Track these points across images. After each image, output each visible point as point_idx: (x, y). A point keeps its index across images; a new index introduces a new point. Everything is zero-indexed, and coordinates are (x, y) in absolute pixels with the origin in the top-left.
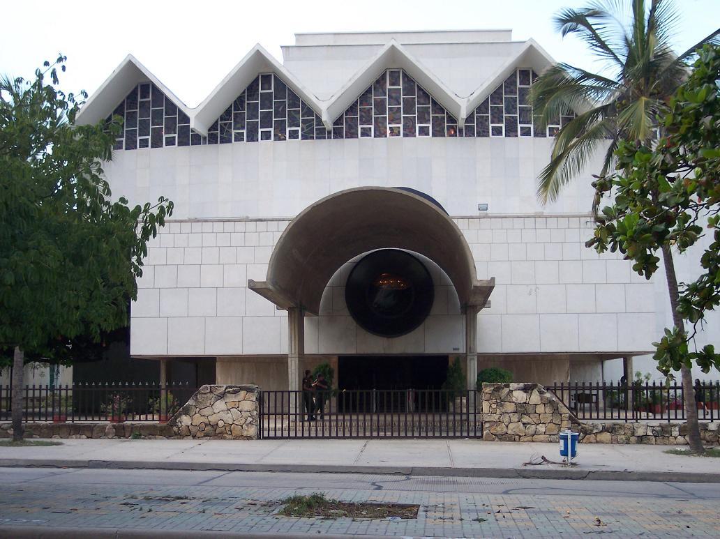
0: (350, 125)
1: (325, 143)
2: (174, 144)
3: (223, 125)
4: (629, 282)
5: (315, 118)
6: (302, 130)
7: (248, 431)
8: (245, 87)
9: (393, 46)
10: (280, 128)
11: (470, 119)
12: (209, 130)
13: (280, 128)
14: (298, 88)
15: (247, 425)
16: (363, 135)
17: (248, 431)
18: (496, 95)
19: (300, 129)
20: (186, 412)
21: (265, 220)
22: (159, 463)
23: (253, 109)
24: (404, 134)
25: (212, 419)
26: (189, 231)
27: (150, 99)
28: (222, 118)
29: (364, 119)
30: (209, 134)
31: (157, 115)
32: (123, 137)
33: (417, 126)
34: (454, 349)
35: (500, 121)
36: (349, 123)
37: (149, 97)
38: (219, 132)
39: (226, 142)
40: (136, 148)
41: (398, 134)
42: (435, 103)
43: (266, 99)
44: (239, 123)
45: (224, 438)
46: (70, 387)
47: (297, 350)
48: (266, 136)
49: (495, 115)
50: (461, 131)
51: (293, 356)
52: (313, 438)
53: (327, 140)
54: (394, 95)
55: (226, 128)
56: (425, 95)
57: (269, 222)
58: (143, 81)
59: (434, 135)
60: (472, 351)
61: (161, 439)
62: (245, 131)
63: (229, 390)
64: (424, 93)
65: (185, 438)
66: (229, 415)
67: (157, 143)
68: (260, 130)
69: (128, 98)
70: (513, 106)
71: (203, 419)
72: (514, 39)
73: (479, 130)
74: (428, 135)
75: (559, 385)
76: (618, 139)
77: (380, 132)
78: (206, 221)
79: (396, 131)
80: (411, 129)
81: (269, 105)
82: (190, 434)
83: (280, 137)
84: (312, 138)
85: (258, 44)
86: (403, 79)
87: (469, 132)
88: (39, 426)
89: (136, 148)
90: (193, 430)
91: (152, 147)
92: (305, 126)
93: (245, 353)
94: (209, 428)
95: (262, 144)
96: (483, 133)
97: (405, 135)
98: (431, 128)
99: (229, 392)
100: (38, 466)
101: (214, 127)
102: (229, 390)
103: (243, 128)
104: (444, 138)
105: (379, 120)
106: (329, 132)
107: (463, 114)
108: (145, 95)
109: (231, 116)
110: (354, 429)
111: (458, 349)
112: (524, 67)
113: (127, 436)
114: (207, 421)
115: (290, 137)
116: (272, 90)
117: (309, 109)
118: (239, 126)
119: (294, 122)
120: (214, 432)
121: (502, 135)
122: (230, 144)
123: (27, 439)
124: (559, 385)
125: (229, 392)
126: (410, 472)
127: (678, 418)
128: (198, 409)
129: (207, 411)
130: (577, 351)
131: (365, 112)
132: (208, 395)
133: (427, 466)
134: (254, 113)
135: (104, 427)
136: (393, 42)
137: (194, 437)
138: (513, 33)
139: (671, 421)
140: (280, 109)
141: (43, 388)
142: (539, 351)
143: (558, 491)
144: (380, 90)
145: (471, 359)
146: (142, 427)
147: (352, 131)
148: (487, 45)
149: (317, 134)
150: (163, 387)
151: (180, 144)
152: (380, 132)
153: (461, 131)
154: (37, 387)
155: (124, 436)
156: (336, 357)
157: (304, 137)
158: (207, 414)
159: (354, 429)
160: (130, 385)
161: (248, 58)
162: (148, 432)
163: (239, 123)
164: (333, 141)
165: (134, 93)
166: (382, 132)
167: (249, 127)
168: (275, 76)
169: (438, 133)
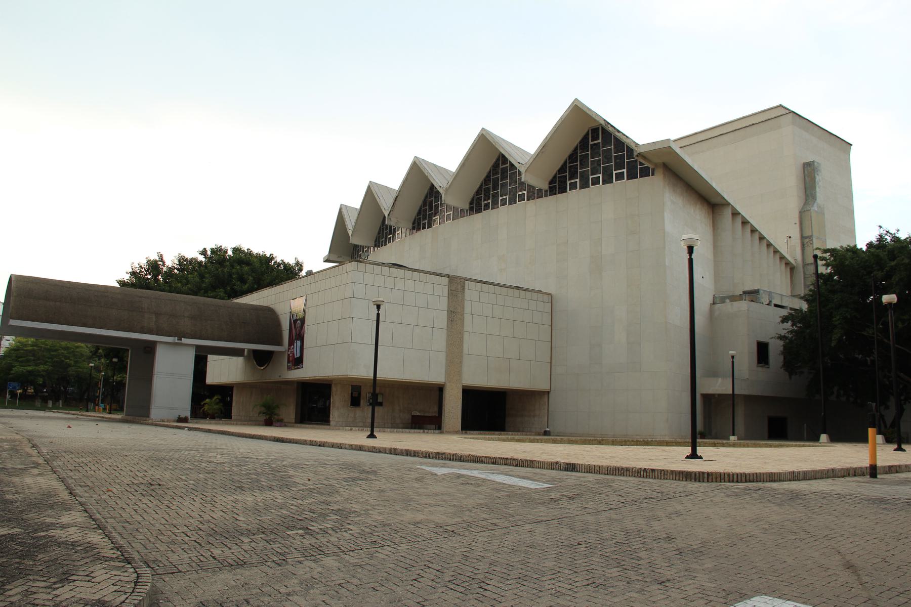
4: (540, 325)
30: (550, 187)
32: (625, 169)
40: (650, 176)
49: (486, 194)
58: (593, 125)
67: (608, 180)
85: (483, 128)
93: (190, 409)
101: (471, 203)
106: (546, 191)
108: (595, 138)
121: (599, 184)
126: (494, 461)
156: (155, 413)
157: (604, 182)
163: (573, 175)
164: (549, 198)
165: (585, 139)
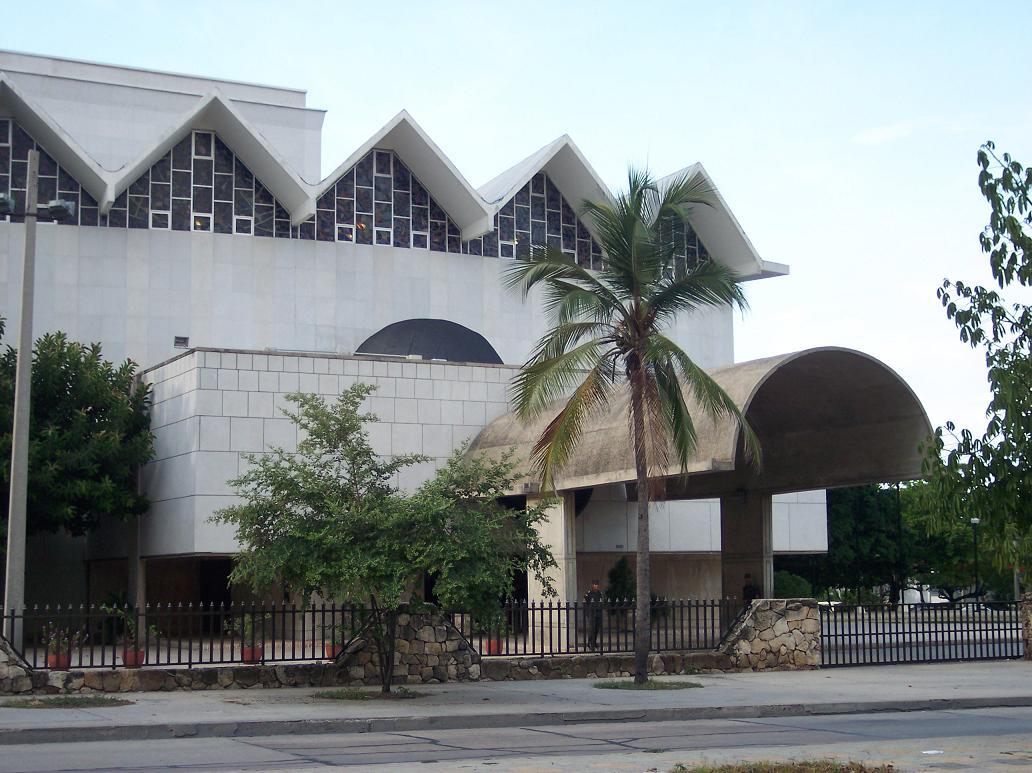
0: (323, 221)
1: (288, 243)
3: (134, 200)
6: (256, 221)
7: (812, 658)
9: (216, 98)
10: (224, 215)
11: (120, 199)
13: (224, 215)
14: (159, 148)
16: (341, 237)
17: (812, 658)
18: (157, 167)
19: (252, 219)
20: (745, 635)
21: (217, 351)
22: (896, 703)
23: (182, 183)
24: (394, 242)
25: (774, 644)
26: (413, 375)
27: (10, 144)
29: (342, 216)
33: (412, 233)
34: (618, 547)
35: (510, 238)
36: (323, 218)
38: (320, 229)
39: (140, 227)
41: (388, 242)
42: (434, 204)
43: (203, 169)
45: (787, 669)
46: (19, 612)
49: (505, 229)
50: (465, 246)
52: (888, 663)
53: (291, 241)
54: (382, 186)
55: (139, 204)
56: (421, 193)
57: (286, 358)
59: (432, 248)
62: (169, 213)
63: (791, 605)
64: (421, 189)
65: (744, 670)
66: (792, 638)
70: (525, 219)
71: (764, 645)
72: (308, 105)
73: (135, 216)
74: (249, 231)
75: (678, 603)
77: (363, 237)
78: (304, 356)
79: (385, 237)
80: (404, 236)
82: (752, 665)
83: (223, 227)
84: (271, 235)
86: (395, 166)
87: (116, 219)
88: (711, 657)
90: (754, 659)
92: (259, 217)
93: (672, 550)
96: (139, 223)
97: (397, 244)
98: (392, 234)
99: (791, 609)
100: (623, 720)
102: (791, 605)
104: (74, 227)
105: (363, 219)
106: (104, 218)
107: (110, 196)
109: (147, 187)
111: (621, 546)
112: (205, 128)
113: (678, 671)
114: (768, 648)
117: (265, 191)
118: (159, 204)
120: (777, 661)
122: (145, 230)
123: (655, 678)
124: (678, 603)
125: (791, 609)
127: (276, 658)
129: (767, 634)
130: (788, 549)
131: (343, 206)
133: (131, 741)
136: (215, 93)
137: (755, 669)
138: (307, 95)
139: (193, 667)
140: (224, 187)
141: (337, 608)
142: (709, 549)
143: (543, 750)
144: (365, 178)
146: (695, 659)
147: (327, 230)
148: (73, 82)
149: (277, 229)
150: (142, 611)
152: (363, 237)
153: (104, 218)
155: (674, 672)
157: (258, 233)
158: (767, 638)
162: (702, 665)
163: (160, 200)
164: (300, 242)
166: (367, 237)
167: (175, 207)
169: (438, 246)
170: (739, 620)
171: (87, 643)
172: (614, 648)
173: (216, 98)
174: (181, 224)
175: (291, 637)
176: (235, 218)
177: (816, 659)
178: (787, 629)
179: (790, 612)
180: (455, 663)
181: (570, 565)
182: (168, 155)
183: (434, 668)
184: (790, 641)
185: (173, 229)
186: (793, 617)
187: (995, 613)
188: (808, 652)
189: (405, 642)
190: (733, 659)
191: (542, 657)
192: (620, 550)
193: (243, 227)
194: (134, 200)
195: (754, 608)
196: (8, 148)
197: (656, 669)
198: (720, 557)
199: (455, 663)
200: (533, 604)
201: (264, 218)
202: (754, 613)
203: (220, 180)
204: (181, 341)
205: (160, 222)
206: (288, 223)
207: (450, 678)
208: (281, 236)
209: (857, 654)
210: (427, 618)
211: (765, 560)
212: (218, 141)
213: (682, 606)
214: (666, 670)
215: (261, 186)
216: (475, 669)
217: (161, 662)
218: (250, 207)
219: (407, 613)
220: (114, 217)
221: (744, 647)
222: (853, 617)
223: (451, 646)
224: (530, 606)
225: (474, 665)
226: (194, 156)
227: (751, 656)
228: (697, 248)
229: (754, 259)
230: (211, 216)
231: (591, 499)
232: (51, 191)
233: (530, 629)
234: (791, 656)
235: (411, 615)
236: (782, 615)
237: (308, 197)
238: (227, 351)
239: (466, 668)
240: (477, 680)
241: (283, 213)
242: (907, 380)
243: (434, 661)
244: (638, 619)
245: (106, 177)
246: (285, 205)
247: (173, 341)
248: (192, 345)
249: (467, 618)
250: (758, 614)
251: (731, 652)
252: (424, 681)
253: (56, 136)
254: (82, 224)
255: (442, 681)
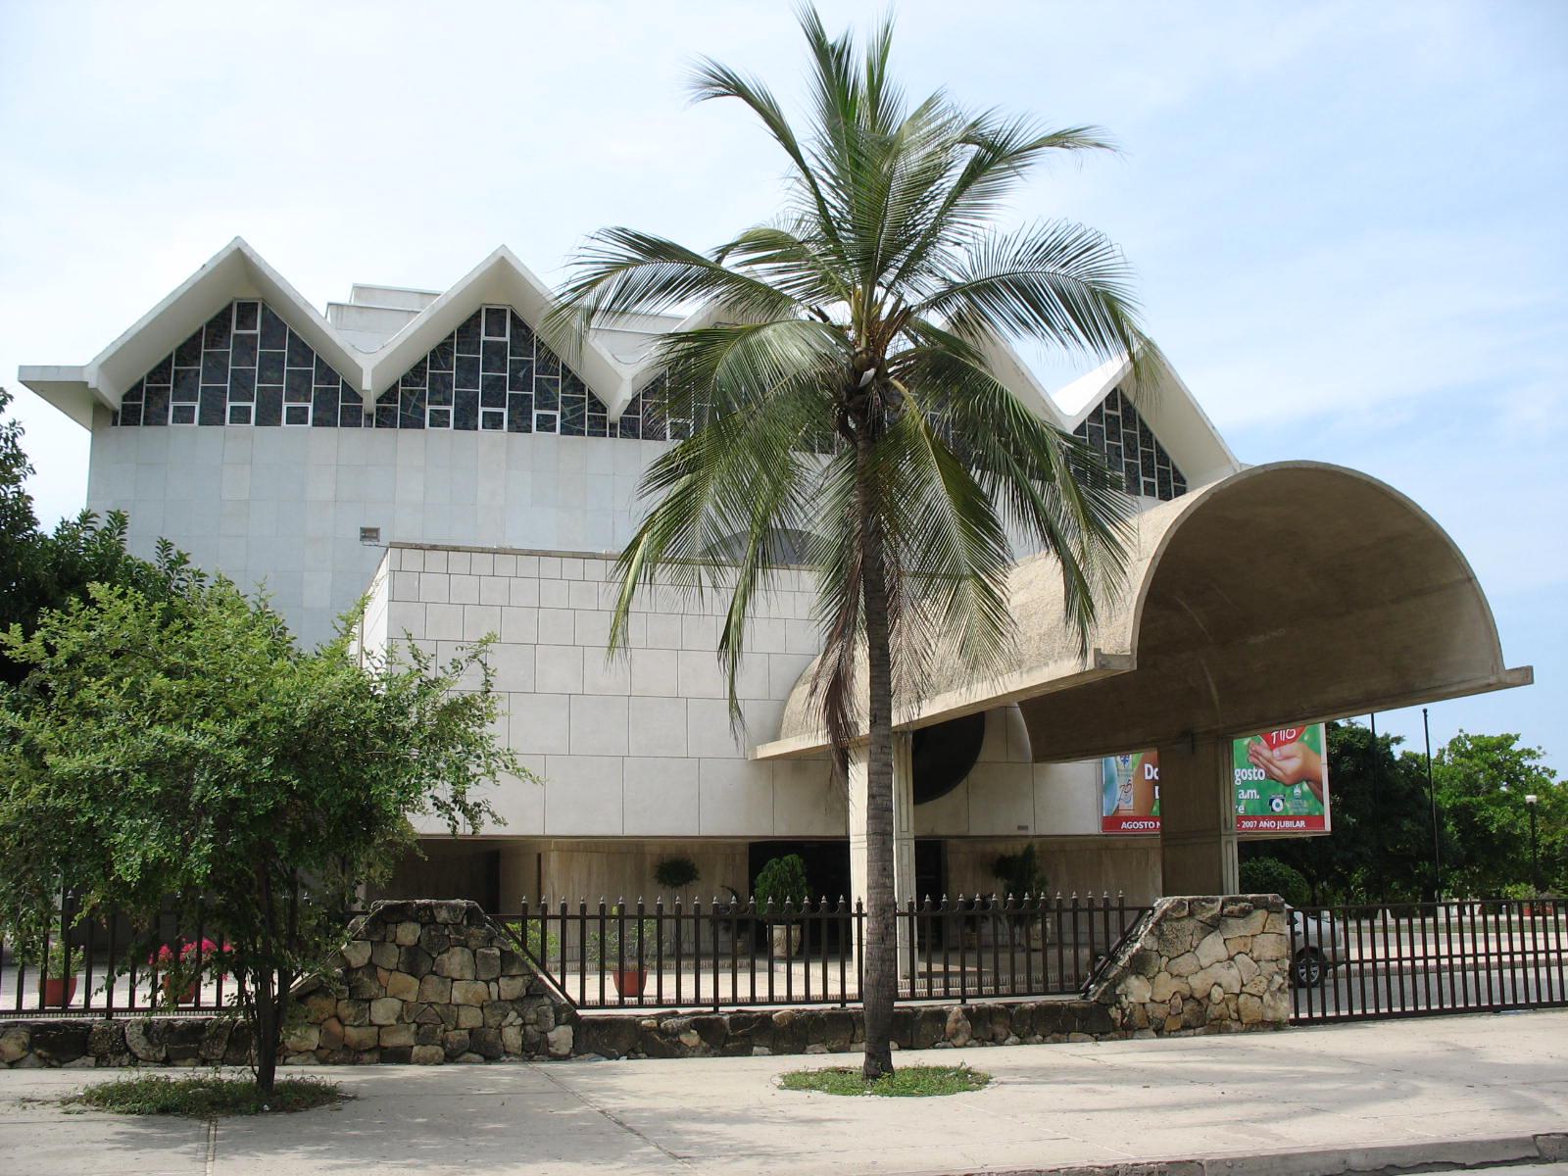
1: (606, 442)
2: (305, 422)
3: (408, 394)
5: (586, 396)
8: (453, 326)
9: (503, 257)
12: (378, 401)
15: (1273, 995)
20: (1140, 965)
23: (468, 369)
25: (1198, 983)
27: (258, 331)
28: (405, 381)
31: (272, 364)
34: (1020, 828)
37: (255, 329)
40: (222, 422)
43: (495, 352)
44: (439, 392)
47: (911, 825)
48: (494, 422)
51: (906, 835)
53: (608, 440)
60: (1229, 826)
61: (992, 1046)
62: (452, 409)
63: (1230, 908)
65: (1137, 1034)
66: (1234, 971)
68: (481, 410)
69: (210, 325)
71: (1176, 985)
76: (128, 588)
81: (499, 364)
83: (520, 425)
84: (581, 433)
87: (384, 418)
89: (222, 422)
91: (257, 424)
92: (567, 410)
94: (1190, 1006)
95: (483, 436)
99: (1231, 915)
102: (1230, 908)
103: (448, 402)
109: (423, 378)
110: (1383, 1001)
111: (1026, 828)
115: (539, 428)
116: (507, 338)
117: (575, 378)
118: (440, 398)
119: (546, 401)
125: (1231, 915)
128: (1165, 960)
129: (1184, 964)
132: (1185, 922)
134: (471, 377)
135: (941, 1016)
137: (1160, 1032)
140: (521, 374)
141: (569, 912)
145: (1227, 843)
149: (590, 426)
151: (317, 422)
154: (593, 910)
158: (1184, 971)
159: (1383, 1001)
160: (814, 905)
161: (484, 269)
167: (459, 401)
168: (512, 312)
170: (1127, 938)
171: (678, 956)
172: (938, 990)
173: (503, 257)
174: (465, 422)
175: (47, 984)
176: (535, 413)
177: (1284, 1008)
178: (1222, 953)
179: (1230, 921)
180: (520, 1021)
181: (905, 848)
182: (451, 336)
183: (471, 1031)
184: (1230, 977)
185: (455, 428)
186: (1237, 928)
187: (1352, 924)
188: (1267, 997)
189: (410, 978)
190: (1114, 1013)
191: (716, 1011)
192: (1023, 833)
193: (546, 424)
194: (408, 394)
195: (1158, 914)
196: (257, 335)
197: (955, 1034)
198: (1158, 843)
199: (520, 1021)
200: (859, 906)
201: (573, 412)
202: (1157, 924)
203: (516, 367)
204: (369, 534)
205: (439, 420)
206: (605, 417)
207: (507, 1054)
208: (595, 434)
209: (1259, 1100)
210: (458, 932)
211: (1224, 840)
212: (514, 317)
213: (1076, 910)
214: (972, 1037)
215: (569, 372)
216: (562, 1036)
217: (25, 1007)
218: (555, 398)
219: (415, 921)
220: (382, 416)
221: (1137, 990)
222: (1378, 923)
223: (512, 987)
224: (854, 910)
225: (561, 1028)
226: (483, 337)
227: (1149, 1006)
228: (1154, 451)
229: (1228, 460)
230: (505, 411)
231: (978, 760)
232: (306, 386)
233: (855, 949)
234: (1232, 1006)
235: (423, 926)
236: (1214, 925)
237: (622, 380)
238: (434, 548)
239: (544, 1033)
240: (565, 1058)
241: (598, 406)
242: (1447, 530)
243: (470, 1018)
244: (1049, 931)
245: (360, 360)
246: (600, 396)
247: (358, 534)
248: (385, 538)
249: (795, 933)
250: (1165, 927)
251: (1112, 998)
252: (450, 1058)
253: (302, 311)
254: (341, 425)
255: (490, 1058)
